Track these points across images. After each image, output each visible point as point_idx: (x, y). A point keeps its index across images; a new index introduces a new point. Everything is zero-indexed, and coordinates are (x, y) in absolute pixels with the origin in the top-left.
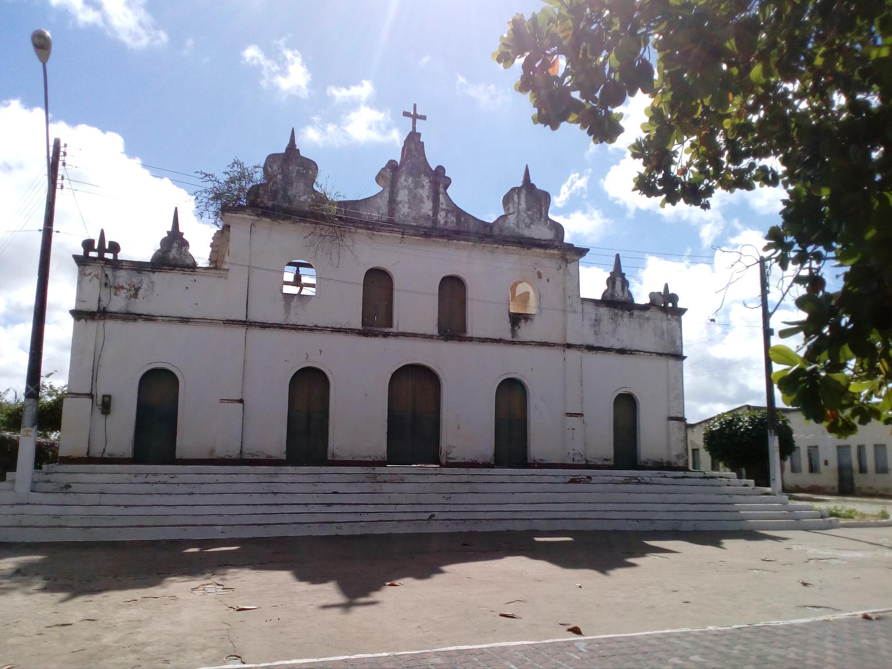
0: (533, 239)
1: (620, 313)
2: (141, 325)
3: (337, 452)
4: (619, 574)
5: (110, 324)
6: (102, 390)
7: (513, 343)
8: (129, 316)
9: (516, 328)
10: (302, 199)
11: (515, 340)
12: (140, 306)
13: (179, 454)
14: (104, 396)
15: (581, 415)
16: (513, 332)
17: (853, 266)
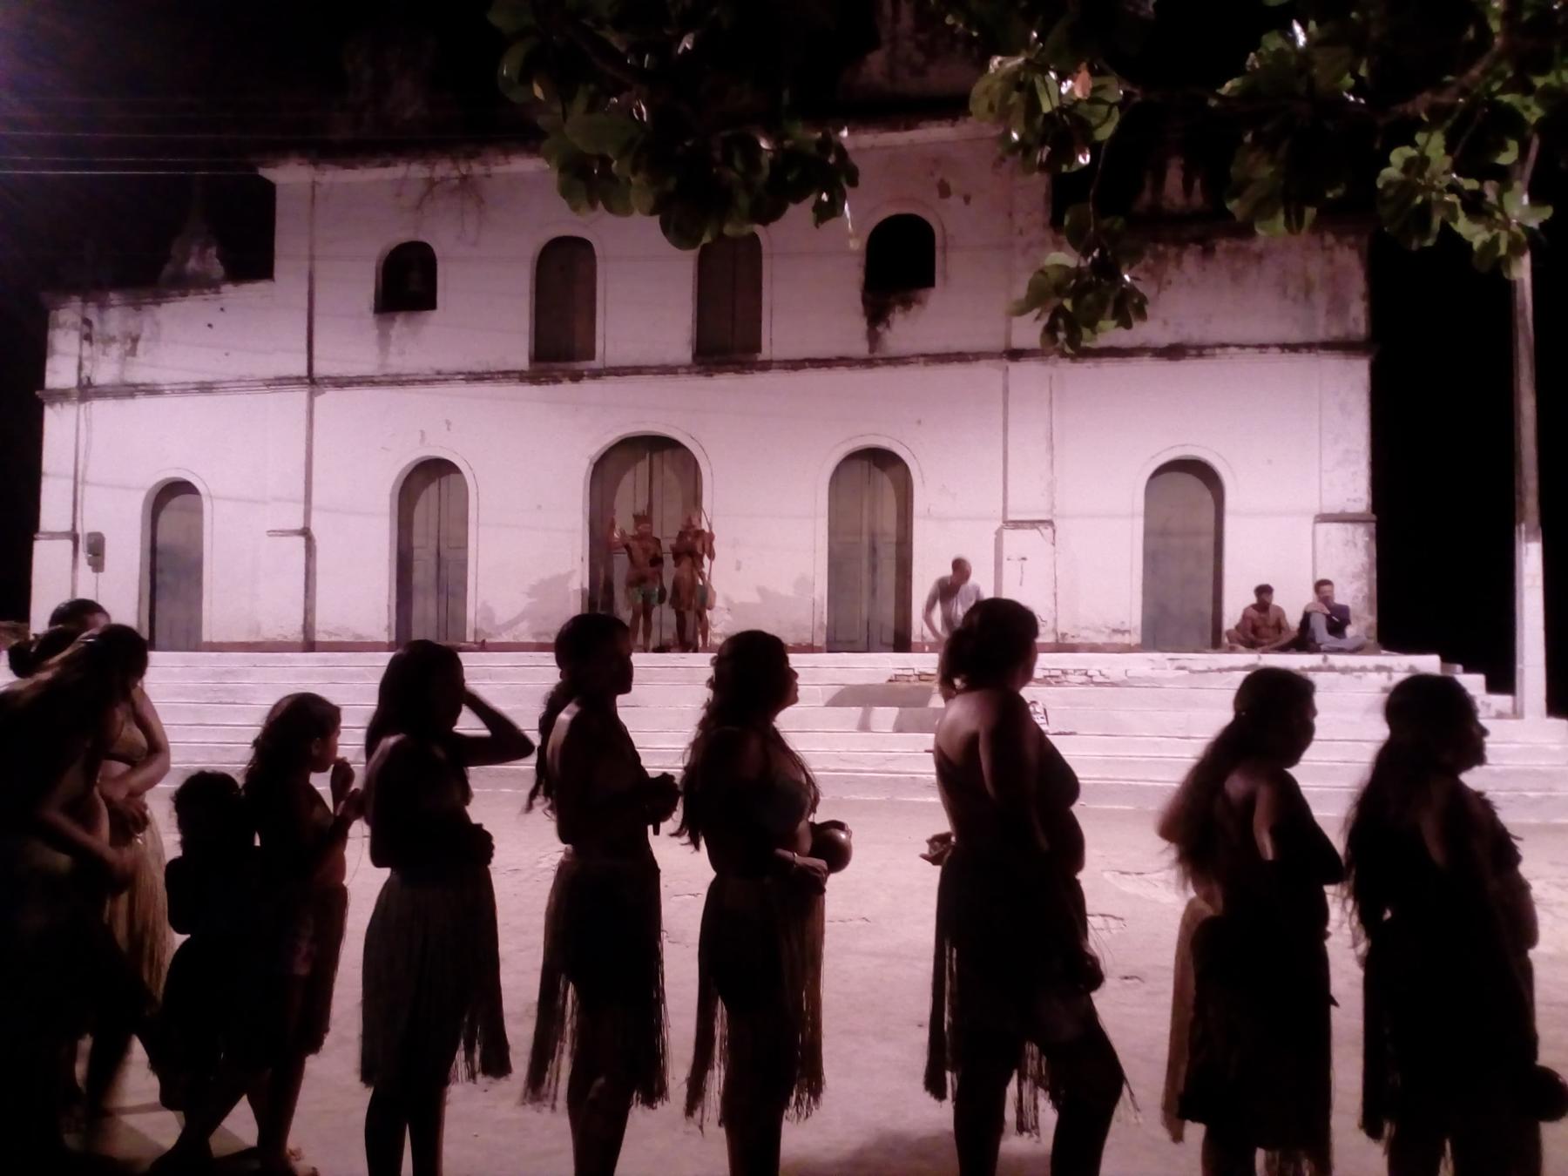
0: (737, 372)
1: (1172, 251)
2: (142, 403)
3: (488, 614)
4: (1489, 795)
5: (98, 407)
6: (86, 527)
7: (869, 363)
8: (128, 390)
9: (880, 329)
10: (408, 114)
11: (877, 354)
12: (140, 373)
13: (206, 638)
14: (90, 535)
15: (1050, 523)
16: (873, 338)
17: (570, 978)
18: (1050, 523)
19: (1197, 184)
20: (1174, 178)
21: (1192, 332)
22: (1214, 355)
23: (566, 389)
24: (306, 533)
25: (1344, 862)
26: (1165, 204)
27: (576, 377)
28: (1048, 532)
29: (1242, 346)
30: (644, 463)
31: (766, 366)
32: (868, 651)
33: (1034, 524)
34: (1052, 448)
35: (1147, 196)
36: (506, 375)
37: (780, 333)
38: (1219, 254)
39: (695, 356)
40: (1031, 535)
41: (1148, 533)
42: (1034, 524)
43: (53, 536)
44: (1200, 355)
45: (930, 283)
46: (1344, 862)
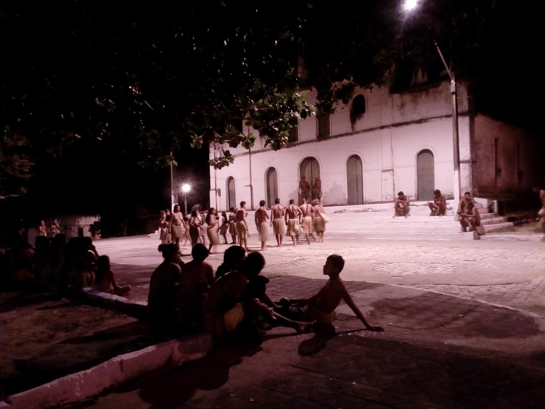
7: (351, 134)
16: (353, 127)
18: (392, 170)
19: (425, 75)
20: (420, 74)
21: (425, 115)
22: (429, 121)
23: (293, 148)
24: (251, 186)
25: (214, 273)
26: (418, 82)
27: (295, 146)
28: (392, 172)
29: (435, 118)
30: (309, 163)
31: (330, 138)
32: (357, 204)
33: (388, 170)
34: (392, 150)
35: (413, 80)
36: (311, 141)
37: (334, 130)
38: (430, 93)
39: (317, 137)
40: (388, 173)
41: (418, 170)
42: (388, 170)
43: (213, 190)
44: (426, 122)
45: (365, 112)
46: (214, 273)
